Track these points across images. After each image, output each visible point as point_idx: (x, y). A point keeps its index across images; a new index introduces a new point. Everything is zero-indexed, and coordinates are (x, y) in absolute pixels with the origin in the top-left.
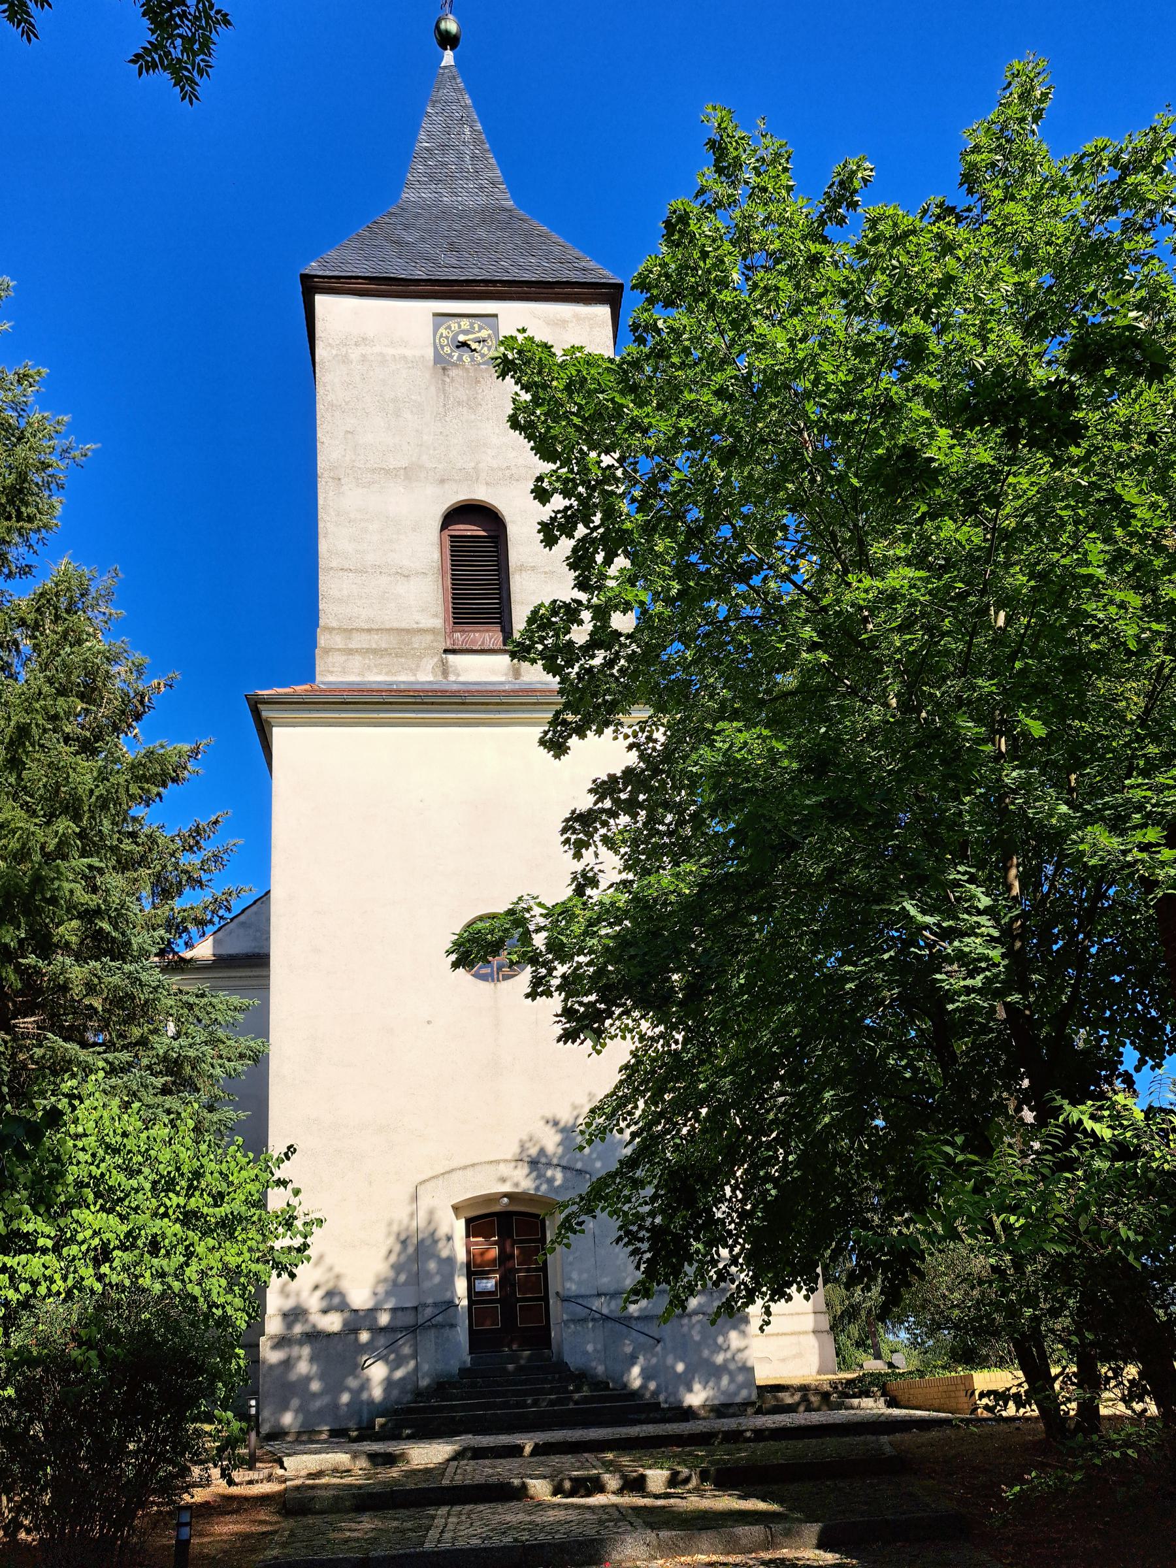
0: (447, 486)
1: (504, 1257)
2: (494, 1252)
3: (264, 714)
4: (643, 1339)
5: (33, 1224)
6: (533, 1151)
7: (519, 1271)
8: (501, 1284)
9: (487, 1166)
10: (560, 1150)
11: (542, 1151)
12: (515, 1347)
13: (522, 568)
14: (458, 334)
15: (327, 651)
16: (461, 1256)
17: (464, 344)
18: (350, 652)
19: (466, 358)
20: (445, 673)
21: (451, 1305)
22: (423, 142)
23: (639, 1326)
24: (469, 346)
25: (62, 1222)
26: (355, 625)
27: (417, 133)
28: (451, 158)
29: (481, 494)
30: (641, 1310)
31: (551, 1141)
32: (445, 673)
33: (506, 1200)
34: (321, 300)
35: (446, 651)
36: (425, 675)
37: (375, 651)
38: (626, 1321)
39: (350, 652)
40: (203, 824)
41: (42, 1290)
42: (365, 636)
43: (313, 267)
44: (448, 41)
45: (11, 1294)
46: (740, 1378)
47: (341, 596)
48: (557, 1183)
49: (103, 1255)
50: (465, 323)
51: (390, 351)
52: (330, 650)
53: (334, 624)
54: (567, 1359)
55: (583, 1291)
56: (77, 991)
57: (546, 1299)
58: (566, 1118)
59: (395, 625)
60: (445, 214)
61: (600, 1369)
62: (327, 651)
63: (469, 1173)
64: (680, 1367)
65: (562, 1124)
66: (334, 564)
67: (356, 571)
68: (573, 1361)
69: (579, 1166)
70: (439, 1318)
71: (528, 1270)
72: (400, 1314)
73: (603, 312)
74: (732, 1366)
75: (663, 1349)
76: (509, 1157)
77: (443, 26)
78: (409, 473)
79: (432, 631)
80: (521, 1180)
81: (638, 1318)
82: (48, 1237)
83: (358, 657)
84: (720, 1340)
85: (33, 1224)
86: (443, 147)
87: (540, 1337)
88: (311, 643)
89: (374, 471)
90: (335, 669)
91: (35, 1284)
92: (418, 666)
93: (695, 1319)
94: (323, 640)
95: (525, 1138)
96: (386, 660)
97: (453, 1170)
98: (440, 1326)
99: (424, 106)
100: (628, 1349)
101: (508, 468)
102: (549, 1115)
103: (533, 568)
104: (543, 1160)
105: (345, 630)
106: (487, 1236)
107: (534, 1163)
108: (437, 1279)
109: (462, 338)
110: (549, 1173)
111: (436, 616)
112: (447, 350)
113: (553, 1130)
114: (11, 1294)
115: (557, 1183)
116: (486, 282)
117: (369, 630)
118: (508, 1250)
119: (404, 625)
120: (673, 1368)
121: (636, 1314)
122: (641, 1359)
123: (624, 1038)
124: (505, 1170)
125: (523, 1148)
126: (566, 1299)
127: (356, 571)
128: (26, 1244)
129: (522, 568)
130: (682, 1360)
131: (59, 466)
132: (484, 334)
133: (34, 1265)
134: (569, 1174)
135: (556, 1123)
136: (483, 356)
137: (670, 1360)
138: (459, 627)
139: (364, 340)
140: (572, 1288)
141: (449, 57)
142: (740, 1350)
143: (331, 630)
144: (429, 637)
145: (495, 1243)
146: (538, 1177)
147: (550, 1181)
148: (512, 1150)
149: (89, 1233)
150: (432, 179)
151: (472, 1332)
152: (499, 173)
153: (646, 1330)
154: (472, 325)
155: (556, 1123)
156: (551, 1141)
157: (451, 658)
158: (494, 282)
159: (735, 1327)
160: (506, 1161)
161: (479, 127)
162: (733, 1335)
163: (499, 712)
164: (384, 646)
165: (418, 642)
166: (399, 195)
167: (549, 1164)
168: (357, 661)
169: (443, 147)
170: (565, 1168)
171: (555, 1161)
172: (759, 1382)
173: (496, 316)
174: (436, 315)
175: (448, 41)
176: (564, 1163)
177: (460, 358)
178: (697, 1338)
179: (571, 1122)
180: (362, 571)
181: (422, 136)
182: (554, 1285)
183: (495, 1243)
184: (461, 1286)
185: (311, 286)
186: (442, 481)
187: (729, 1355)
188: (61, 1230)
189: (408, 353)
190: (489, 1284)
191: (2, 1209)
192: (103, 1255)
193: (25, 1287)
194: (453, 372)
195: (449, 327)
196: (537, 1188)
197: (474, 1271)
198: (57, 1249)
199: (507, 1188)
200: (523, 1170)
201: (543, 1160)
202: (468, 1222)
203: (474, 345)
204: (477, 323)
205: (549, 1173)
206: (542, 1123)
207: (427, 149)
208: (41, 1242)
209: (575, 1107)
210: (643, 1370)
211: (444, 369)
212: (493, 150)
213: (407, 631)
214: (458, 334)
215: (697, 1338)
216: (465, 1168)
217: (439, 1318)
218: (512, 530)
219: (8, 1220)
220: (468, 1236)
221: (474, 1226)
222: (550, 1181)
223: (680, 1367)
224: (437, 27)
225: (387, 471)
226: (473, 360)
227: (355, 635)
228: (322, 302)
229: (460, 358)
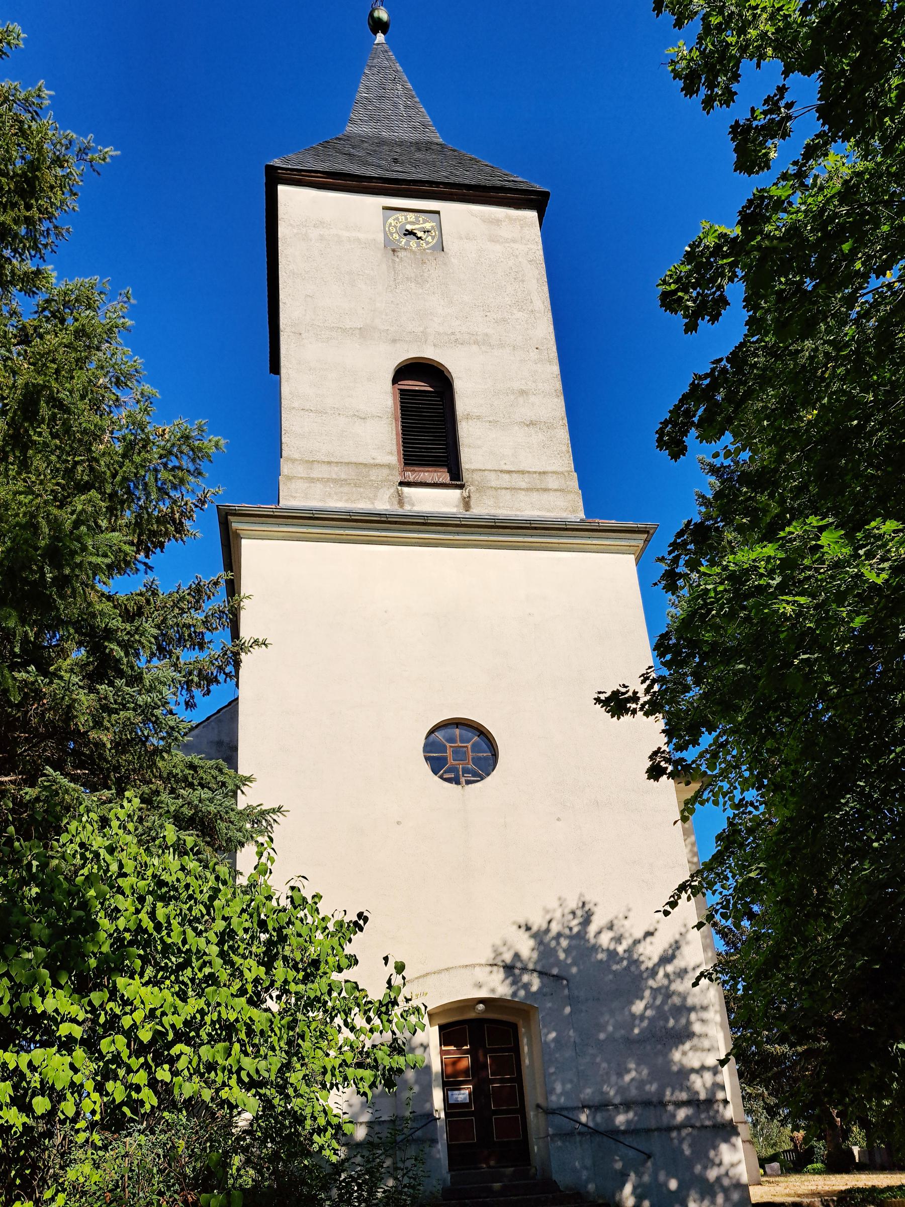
0: (398, 345)
1: (477, 1068)
2: (466, 1062)
3: (235, 526)
4: (631, 1153)
5: (57, 1002)
6: (508, 957)
7: (494, 1081)
8: (473, 1095)
9: (463, 970)
10: (535, 955)
11: (517, 956)
12: (492, 1163)
13: (468, 417)
14: (405, 224)
15: (289, 478)
16: (436, 1067)
17: (410, 233)
18: (312, 480)
19: (413, 242)
20: (401, 503)
21: (430, 1118)
22: (362, 93)
23: (628, 1140)
24: (415, 234)
25: (96, 997)
26: (316, 458)
27: (358, 87)
28: (387, 105)
29: (429, 353)
30: (628, 1122)
31: (526, 947)
32: (401, 503)
33: (481, 1007)
34: (284, 191)
35: (402, 484)
36: (383, 504)
37: (335, 481)
38: (614, 1134)
39: (312, 480)
40: (205, 581)
41: (68, 1108)
42: (325, 468)
43: (276, 162)
44: (378, 26)
45: (15, 1118)
46: (736, 1196)
47: (299, 431)
48: (535, 988)
49: (157, 1050)
50: (411, 216)
51: (346, 234)
52: (293, 478)
53: (296, 456)
54: (555, 1177)
55: (570, 1104)
56: (83, 721)
57: (522, 1111)
58: (538, 922)
59: (354, 460)
60: (382, 142)
61: (591, 1187)
62: (289, 478)
63: (445, 976)
64: (673, 1184)
65: (535, 929)
66: (296, 405)
67: (316, 411)
68: (562, 1179)
69: (555, 971)
70: (419, 1133)
71: (502, 1081)
72: (377, 1128)
73: (533, 215)
74: (726, 1182)
75: (654, 1164)
76: (483, 961)
77: (376, 14)
78: (364, 333)
79: (389, 466)
80: (497, 986)
81: (624, 1132)
82: (74, 1021)
83: (319, 485)
84: (712, 1153)
85: (57, 1002)
86: (380, 98)
87: (518, 1151)
88: (275, 471)
89: (332, 329)
90: (294, 495)
91: (57, 1097)
92: (375, 496)
93: (684, 1132)
94: (286, 468)
95: (499, 942)
96: (346, 489)
97: (427, 974)
98: (419, 1141)
99: (363, 68)
100: (618, 1165)
101: (453, 333)
102: (522, 922)
103: (478, 418)
104: (519, 965)
105: (307, 461)
106: (459, 1045)
107: (509, 969)
108: (416, 1089)
109: (409, 227)
110: (526, 978)
111: (391, 453)
112: (396, 236)
113: (527, 935)
114: (15, 1118)
115: (535, 988)
116: (431, 183)
117: (329, 463)
118: (481, 1058)
119: (361, 460)
120: (666, 1185)
121: (622, 1128)
122: (633, 1176)
123: (716, 803)
124: (481, 974)
125: (498, 954)
126: (549, 1112)
127: (316, 411)
128: (42, 1030)
129: (468, 417)
130: (673, 1177)
131: (75, 169)
132: (428, 226)
133: (55, 1065)
134: (546, 979)
135: (528, 928)
136: (428, 243)
137: (662, 1177)
138: (408, 468)
139: (320, 224)
140: (557, 1099)
141: (380, 38)
142: (732, 1165)
143: (293, 461)
144: (386, 471)
145: (467, 1052)
146: (514, 983)
147: (526, 986)
148: (487, 955)
149: (139, 1016)
150: (371, 118)
151: (450, 1147)
152: (428, 118)
153: (635, 1145)
154: (417, 218)
155: (528, 928)
156: (526, 947)
157: (406, 490)
158: (438, 184)
159: (727, 1140)
160: (481, 965)
161: (409, 86)
162: (724, 1148)
163: (458, 533)
164: (343, 476)
165: (374, 474)
166: (344, 127)
167: (524, 969)
168: (318, 488)
169: (380, 98)
170: (541, 974)
171: (531, 966)
172: (753, 1202)
173: (438, 213)
174: (386, 208)
175: (378, 26)
176: (538, 968)
177: (408, 243)
178: (687, 1152)
179: (544, 926)
180: (321, 412)
181: (361, 88)
182: (533, 1094)
183: (467, 1052)
184: (438, 1096)
185: (275, 178)
186: (394, 341)
187: (722, 1170)
188: (93, 1010)
189: (361, 236)
190: (463, 1095)
191: (7, 974)
192: (157, 1050)
193: (41, 1104)
194: (402, 254)
195: (397, 219)
196: (514, 994)
197: (450, 1083)
198: (90, 1044)
199: (484, 994)
200: (500, 974)
201: (519, 965)
202: (442, 1028)
203: (420, 234)
204: (422, 217)
205: (526, 978)
206: (515, 927)
207: (366, 98)
208: (64, 1029)
209: (547, 911)
210: (635, 1188)
211: (394, 251)
212: (422, 101)
213: (365, 465)
214: (405, 224)
215: (687, 1152)
216: (439, 972)
217: (419, 1133)
218: (459, 386)
219: (16, 990)
220: (441, 1045)
221: (448, 1035)
222: (526, 986)
223: (673, 1184)
224: (371, 15)
225: (344, 330)
226: (418, 245)
227: (316, 465)
228: (284, 191)
229: (408, 243)
